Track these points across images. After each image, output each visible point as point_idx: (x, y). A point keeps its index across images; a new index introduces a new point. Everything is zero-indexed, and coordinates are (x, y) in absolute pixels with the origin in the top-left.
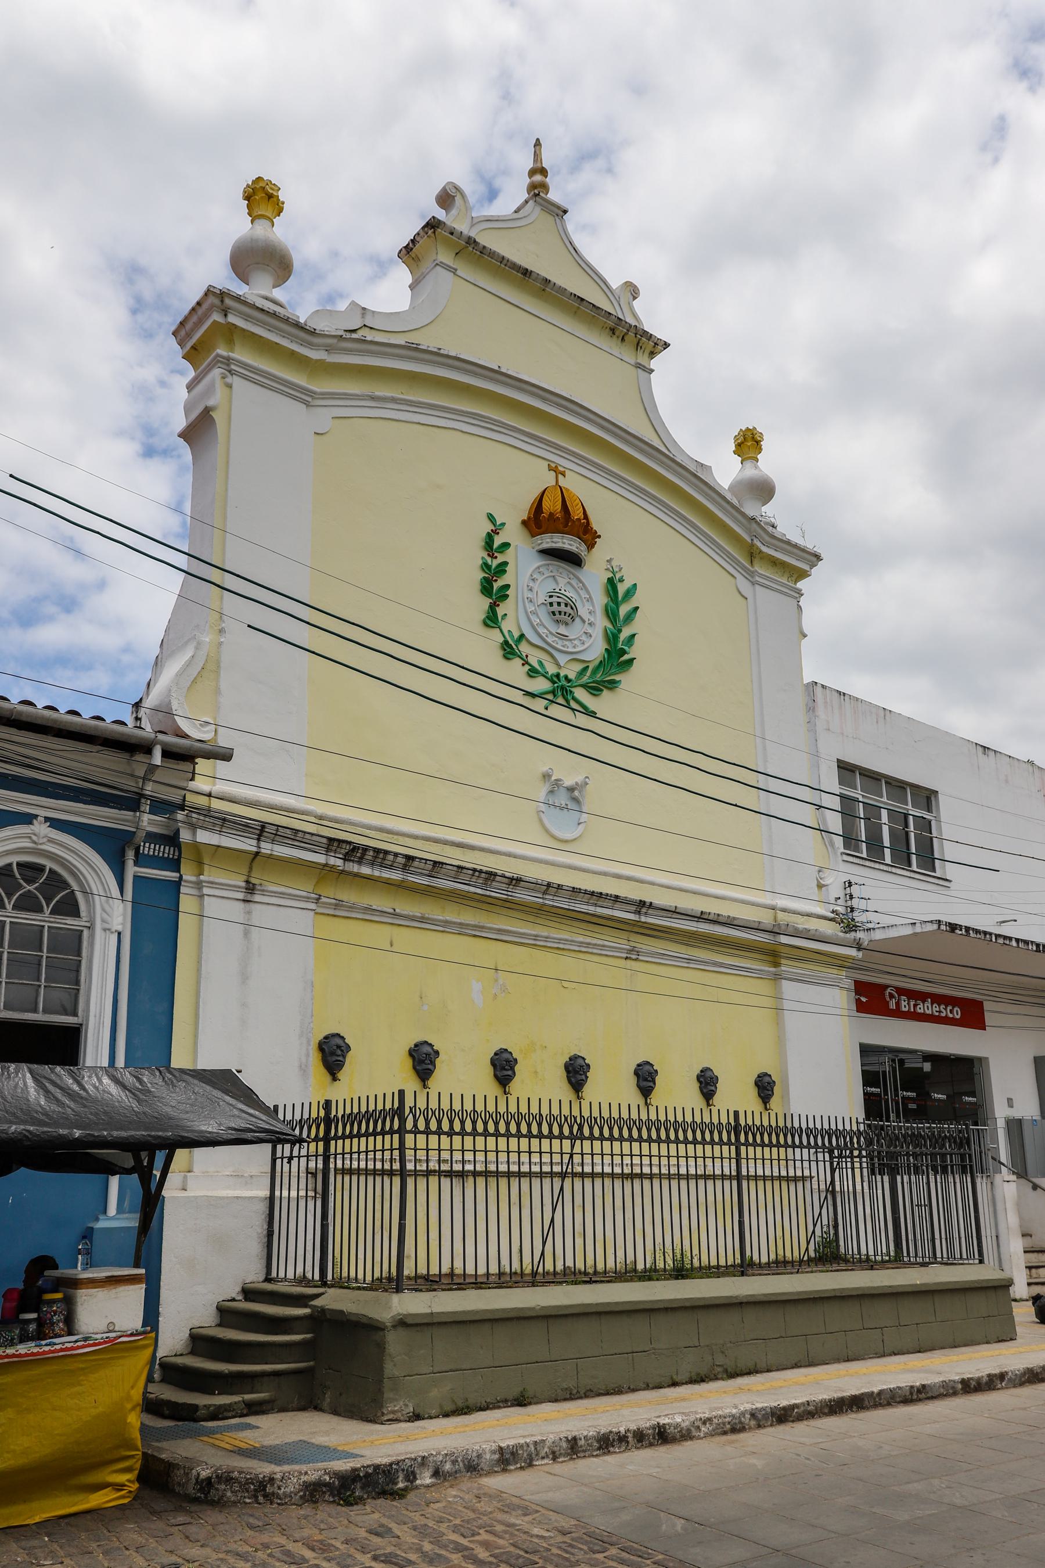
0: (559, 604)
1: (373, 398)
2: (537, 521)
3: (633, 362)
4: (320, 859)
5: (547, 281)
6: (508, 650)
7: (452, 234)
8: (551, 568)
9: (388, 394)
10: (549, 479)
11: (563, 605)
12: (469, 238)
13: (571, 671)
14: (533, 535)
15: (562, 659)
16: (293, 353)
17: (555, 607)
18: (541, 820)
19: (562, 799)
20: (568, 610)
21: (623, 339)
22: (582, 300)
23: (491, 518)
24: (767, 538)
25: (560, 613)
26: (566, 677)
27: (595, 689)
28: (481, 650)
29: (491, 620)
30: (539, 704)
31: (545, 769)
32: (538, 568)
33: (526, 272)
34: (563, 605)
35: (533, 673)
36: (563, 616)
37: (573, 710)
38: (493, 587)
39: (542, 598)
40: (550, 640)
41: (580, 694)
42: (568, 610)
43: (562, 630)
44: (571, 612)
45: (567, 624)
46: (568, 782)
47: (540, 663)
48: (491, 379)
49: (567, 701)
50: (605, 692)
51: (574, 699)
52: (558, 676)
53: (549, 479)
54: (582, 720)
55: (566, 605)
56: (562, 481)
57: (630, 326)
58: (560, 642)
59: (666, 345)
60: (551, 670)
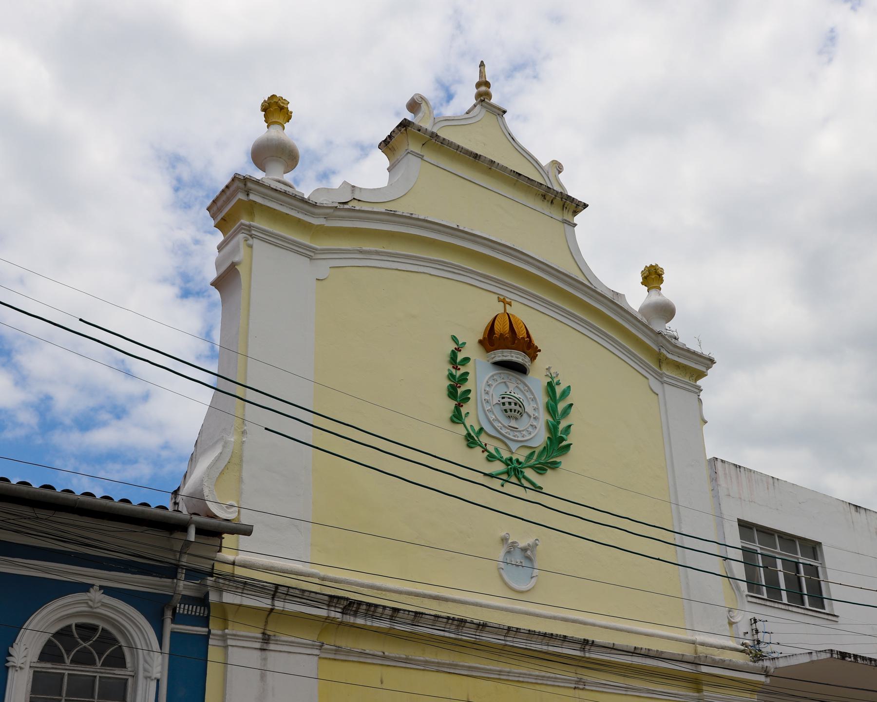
0: (510, 403)
1: (361, 252)
2: (491, 340)
3: (560, 218)
4: (323, 613)
5: (492, 162)
6: (471, 441)
7: (419, 130)
8: (502, 376)
9: (373, 248)
10: (499, 308)
11: (513, 405)
12: (433, 133)
13: (521, 455)
14: (488, 351)
15: (514, 446)
16: (299, 221)
17: (507, 406)
18: (501, 576)
19: (518, 558)
20: (517, 408)
21: (552, 202)
22: (520, 174)
23: (454, 339)
24: (671, 347)
25: (511, 410)
26: (517, 461)
27: (540, 469)
28: (449, 442)
29: (457, 417)
30: (496, 484)
31: (503, 534)
32: (493, 376)
33: (476, 156)
34: (513, 405)
35: (491, 458)
36: (509, 412)
37: (525, 487)
38: (457, 392)
39: (496, 399)
40: (503, 432)
41: (529, 473)
42: (517, 408)
43: (513, 423)
44: (519, 409)
45: (516, 419)
46: (522, 544)
47: (497, 450)
48: (452, 235)
49: (519, 480)
50: (549, 471)
51: (525, 477)
52: (511, 459)
53: (499, 308)
54: (531, 495)
55: (516, 404)
56: (509, 310)
57: (557, 192)
58: (512, 433)
59: (585, 206)
60: (506, 455)
